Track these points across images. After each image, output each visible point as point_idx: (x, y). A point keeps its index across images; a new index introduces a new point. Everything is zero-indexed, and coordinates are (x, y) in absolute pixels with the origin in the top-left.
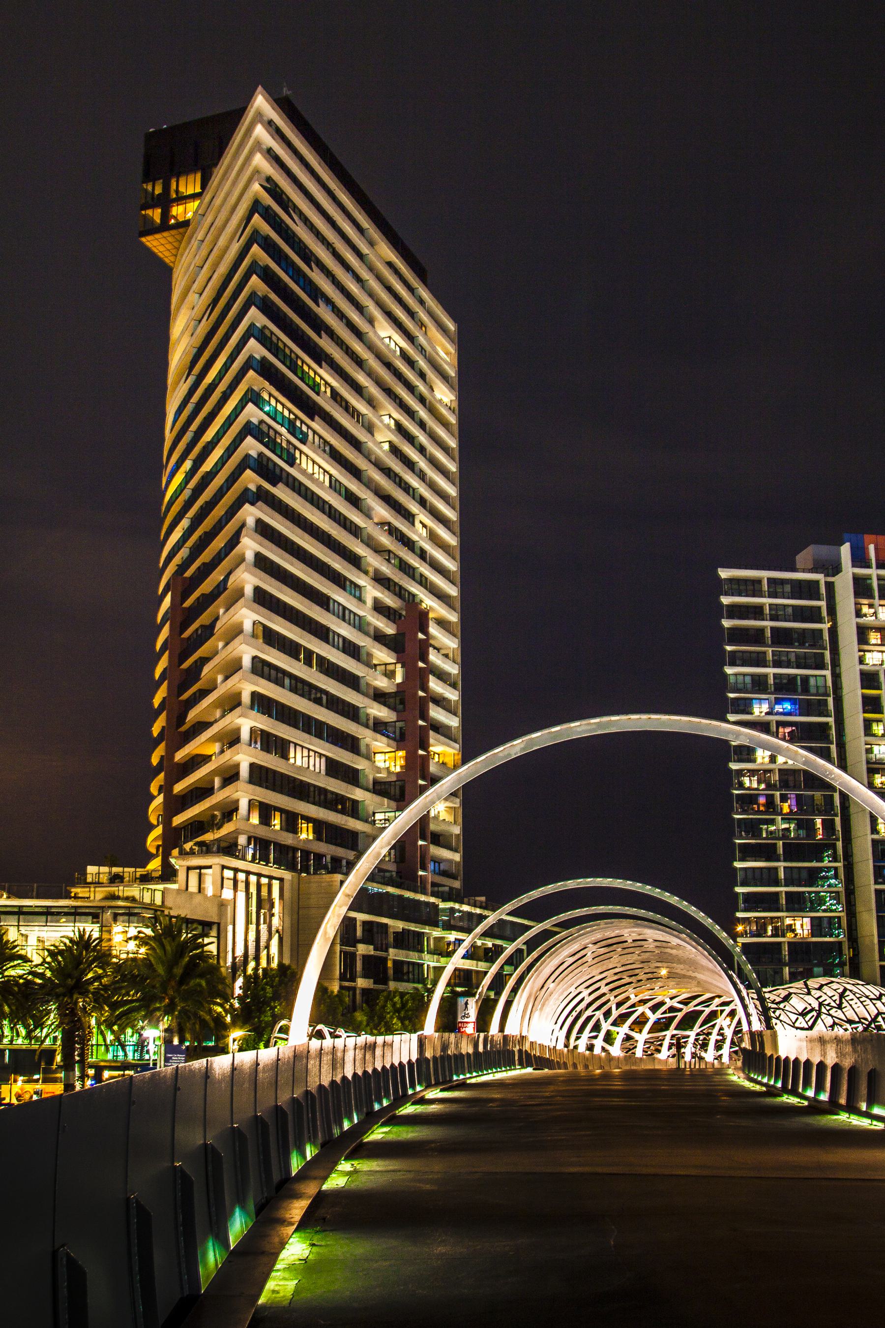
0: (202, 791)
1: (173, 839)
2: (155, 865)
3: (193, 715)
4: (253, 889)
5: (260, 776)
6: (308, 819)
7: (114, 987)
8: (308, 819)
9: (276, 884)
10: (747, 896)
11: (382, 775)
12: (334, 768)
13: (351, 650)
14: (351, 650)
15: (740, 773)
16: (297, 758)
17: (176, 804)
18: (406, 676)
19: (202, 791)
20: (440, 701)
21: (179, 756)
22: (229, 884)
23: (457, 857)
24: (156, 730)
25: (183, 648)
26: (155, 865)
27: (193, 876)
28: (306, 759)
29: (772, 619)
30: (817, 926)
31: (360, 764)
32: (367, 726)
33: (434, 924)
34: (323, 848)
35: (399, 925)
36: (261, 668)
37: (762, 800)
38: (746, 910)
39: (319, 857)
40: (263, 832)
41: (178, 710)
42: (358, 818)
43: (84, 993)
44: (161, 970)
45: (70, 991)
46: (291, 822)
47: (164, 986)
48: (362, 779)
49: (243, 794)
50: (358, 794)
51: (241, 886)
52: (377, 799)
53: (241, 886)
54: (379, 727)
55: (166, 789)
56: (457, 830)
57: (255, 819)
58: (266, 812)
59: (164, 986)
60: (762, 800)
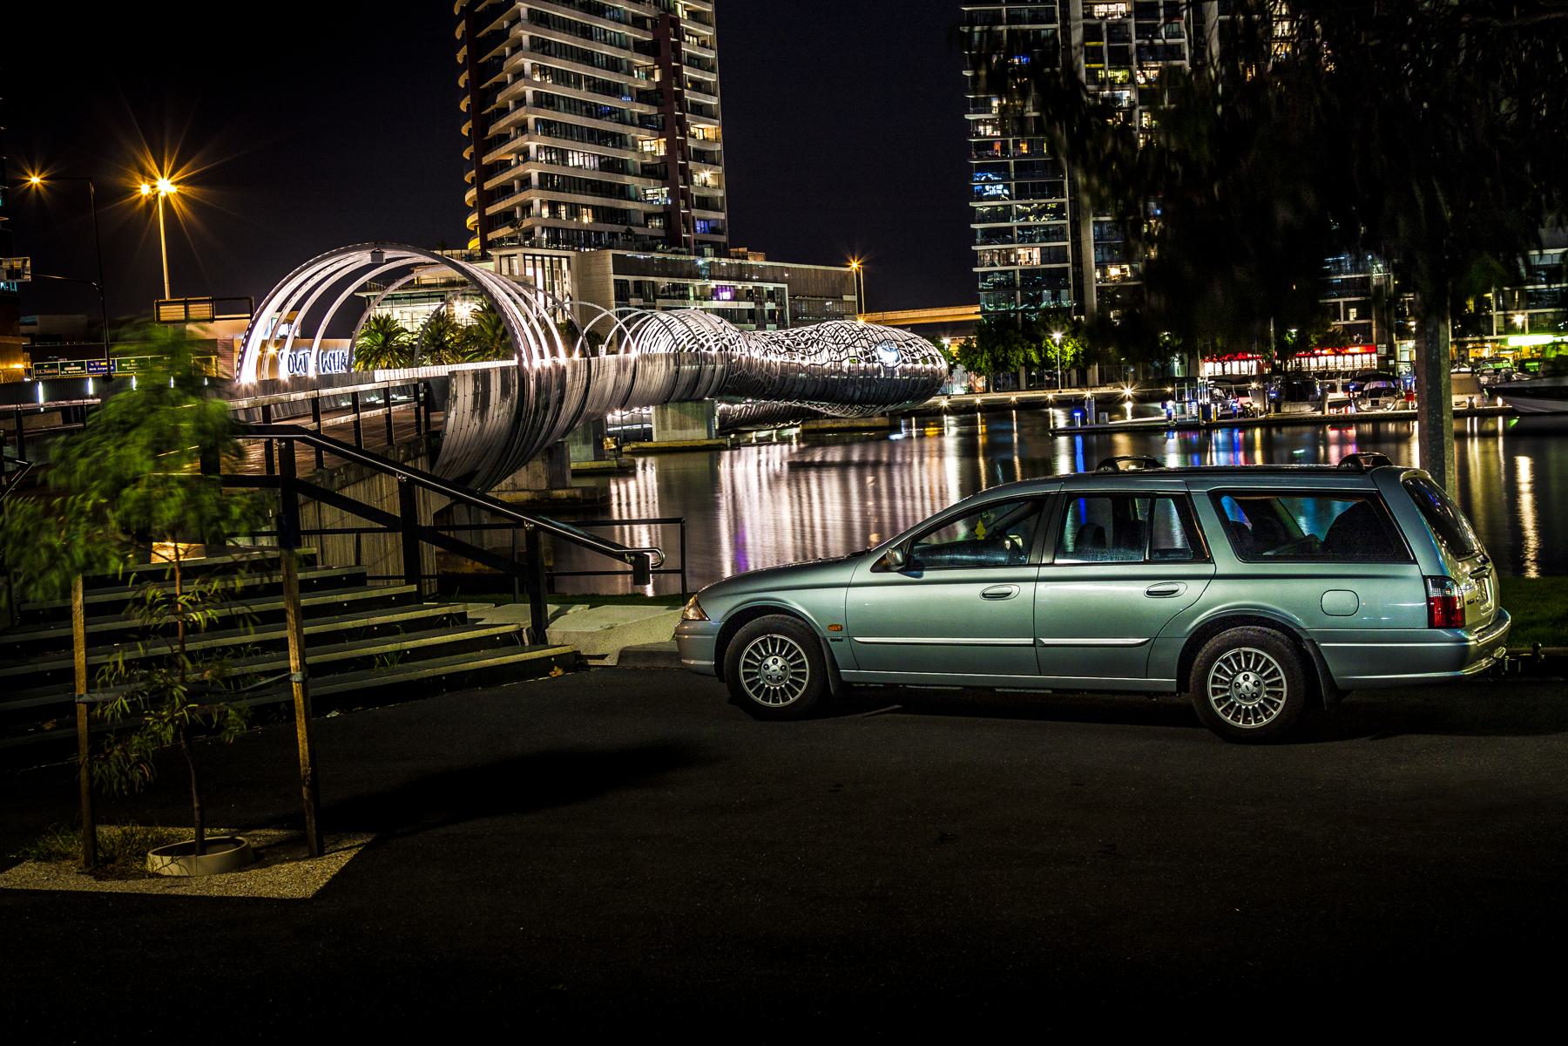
0: (506, 191)
1: (488, 224)
2: (474, 244)
3: (492, 130)
4: (547, 264)
5: (546, 181)
6: (587, 206)
7: (463, 344)
8: (587, 206)
9: (564, 261)
10: (986, 232)
11: (649, 160)
12: (608, 165)
13: (613, 65)
14: (613, 65)
15: (978, 122)
16: (575, 160)
17: (487, 198)
18: (663, 76)
19: (506, 191)
20: (698, 86)
21: (486, 160)
22: (530, 263)
23: (722, 216)
24: (460, 59)
25: (479, 47)
26: (474, 244)
27: (505, 262)
28: (581, 159)
29: (92, 670)
30: (1046, 255)
31: (629, 156)
32: (632, 124)
33: (698, 276)
34: (601, 227)
35: (664, 282)
36: (543, 101)
37: (997, 146)
38: (982, 244)
39: (598, 234)
40: (554, 223)
41: (483, 98)
42: (630, 199)
43: (446, 349)
44: (489, 332)
45: (438, 348)
46: (574, 211)
47: (492, 341)
48: (631, 167)
49: (536, 198)
50: (627, 180)
51: (539, 264)
52: (644, 180)
53: (539, 264)
54: (644, 122)
55: (478, 182)
56: (720, 193)
57: (545, 212)
58: (554, 207)
59: (492, 341)
60: (997, 146)
